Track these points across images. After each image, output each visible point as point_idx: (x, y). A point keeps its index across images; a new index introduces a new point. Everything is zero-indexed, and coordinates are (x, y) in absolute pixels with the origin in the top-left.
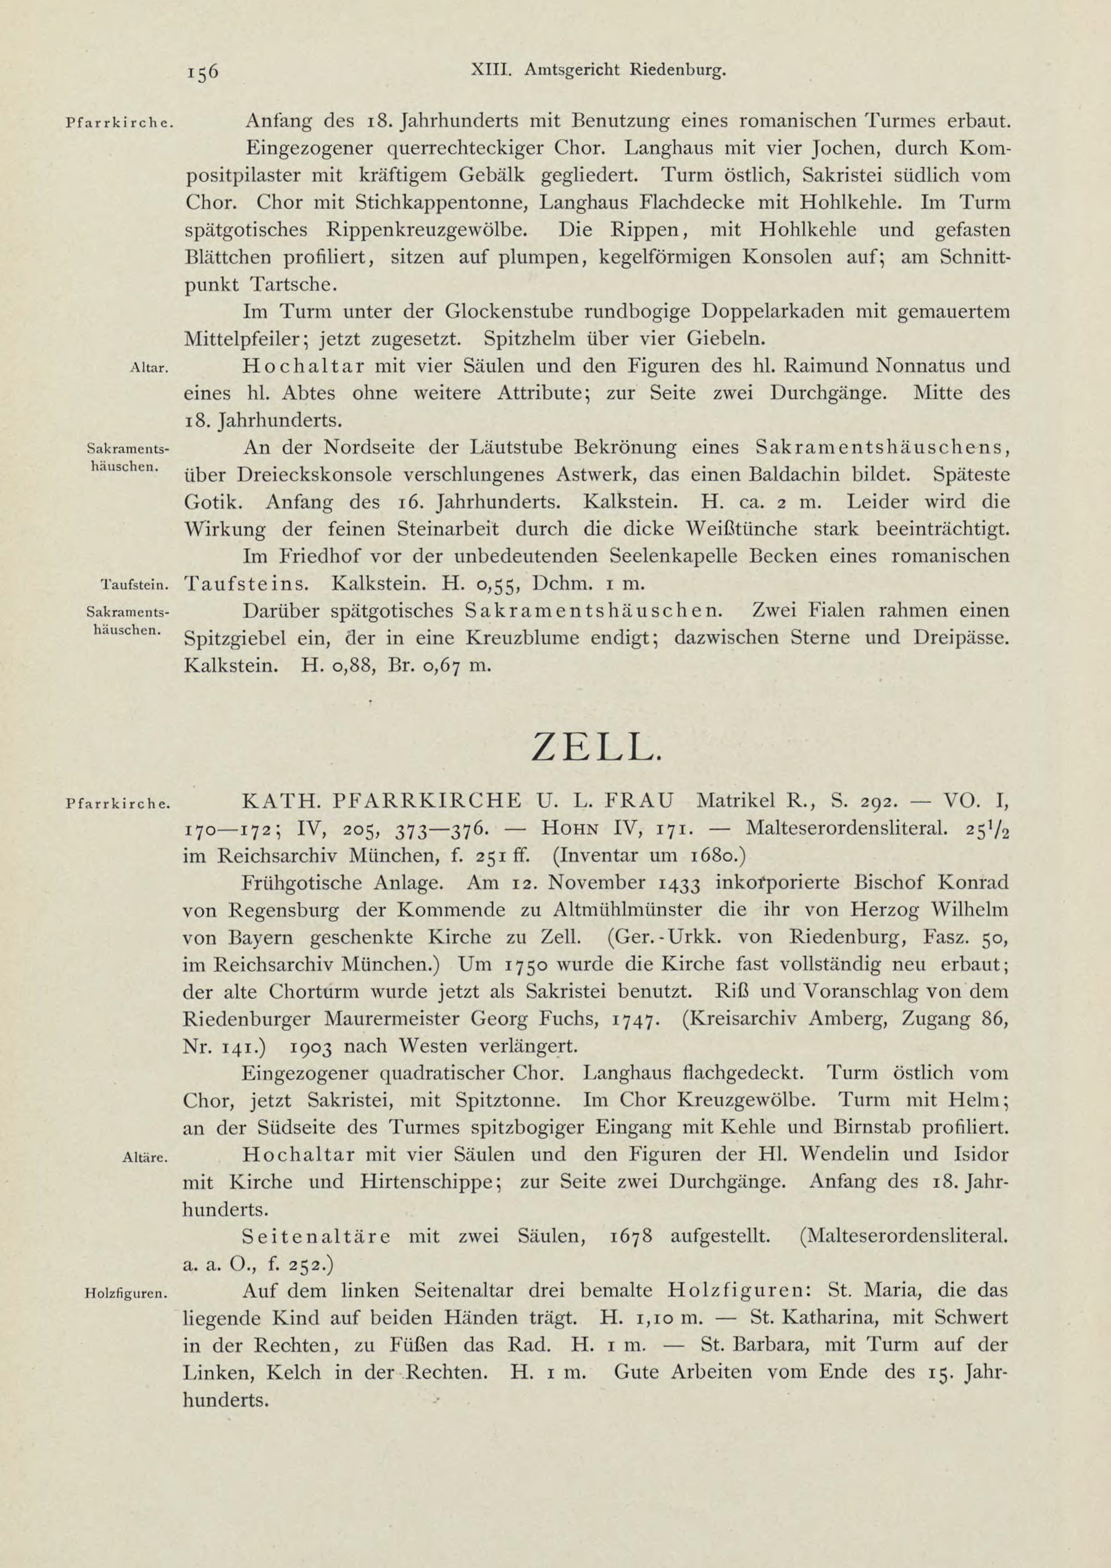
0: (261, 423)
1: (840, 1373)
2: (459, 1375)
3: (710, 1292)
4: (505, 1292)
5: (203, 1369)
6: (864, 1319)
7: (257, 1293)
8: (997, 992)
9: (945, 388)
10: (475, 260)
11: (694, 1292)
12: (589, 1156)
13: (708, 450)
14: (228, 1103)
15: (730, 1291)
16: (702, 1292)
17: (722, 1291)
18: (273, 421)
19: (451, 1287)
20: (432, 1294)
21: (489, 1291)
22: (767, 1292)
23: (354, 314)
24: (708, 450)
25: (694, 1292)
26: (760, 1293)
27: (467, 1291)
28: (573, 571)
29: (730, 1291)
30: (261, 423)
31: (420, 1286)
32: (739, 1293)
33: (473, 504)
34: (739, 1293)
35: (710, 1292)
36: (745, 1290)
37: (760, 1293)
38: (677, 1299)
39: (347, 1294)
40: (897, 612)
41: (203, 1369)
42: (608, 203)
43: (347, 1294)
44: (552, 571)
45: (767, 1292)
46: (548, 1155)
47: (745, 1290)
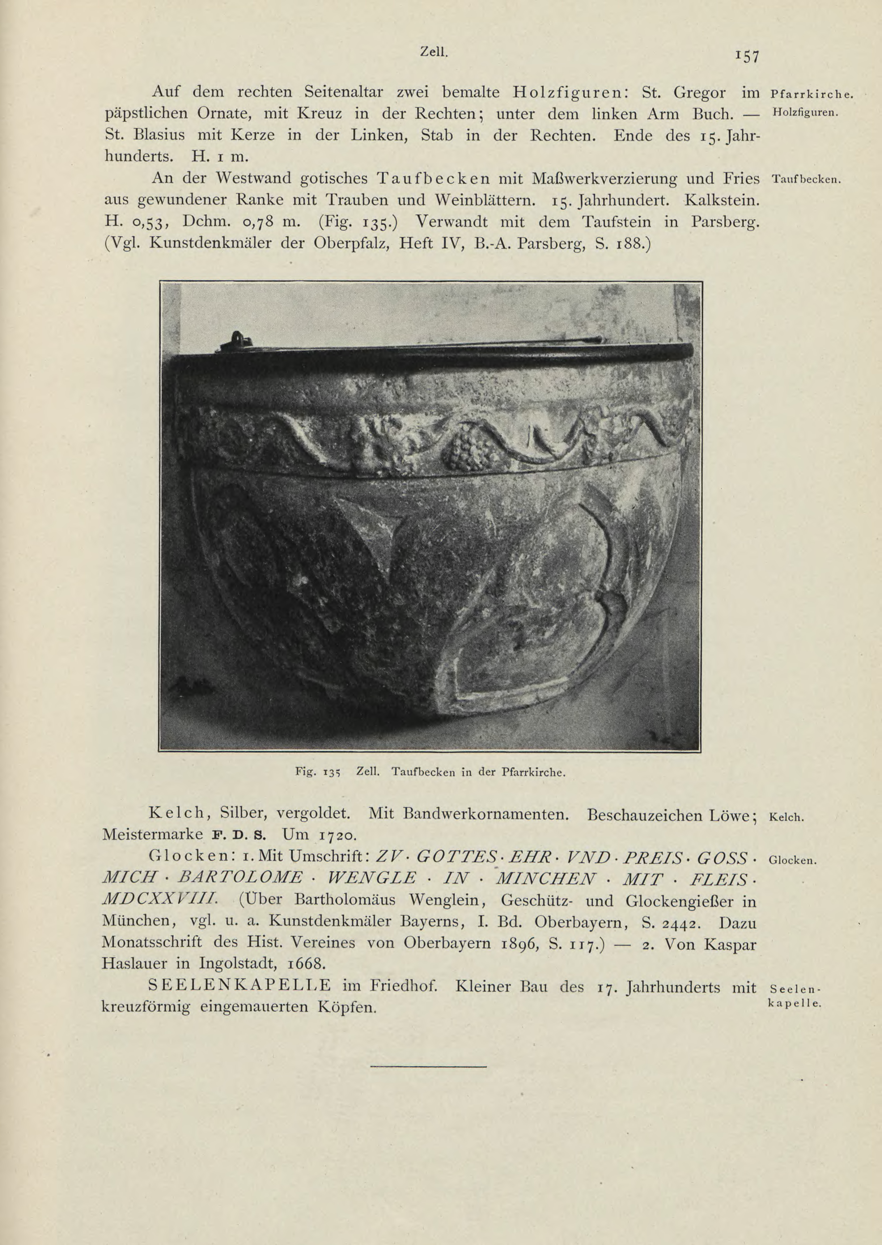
0: (612, 203)
1: (630, 137)
2: (573, 138)
3: (546, 94)
4: (377, 93)
5: (367, 132)
6: (350, 93)
7: (164, 93)
8: (561, 223)
9: (501, 197)
10: (357, 203)
11: (534, 94)
12: (218, 943)
13: (464, 203)
14: (262, 814)
15: (563, 94)
16: (540, 94)
17: (556, 94)
18: (621, 201)
19: (333, 89)
20: (318, 94)
21: (363, 92)
22: (592, 94)
23: (406, 202)
24: (464, 203)
25: (534, 94)
26: (586, 95)
27: (346, 92)
28: (214, 212)
29: (563, 94)
30: (612, 203)
31: (309, 88)
32: (570, 95)
33: (607, 202)
34: (570, 95)
35: (546, 94)
36: (575, 93)
37: (586, 95)
38: (520, 99)
39: (597, 117)
40: (592, 202)
41: (367, 132)
42: (352, 201)
43: (597, 117)
44: (198, 211)
45: (592, 94)
46: (599, 902)
47: (575, 93)
